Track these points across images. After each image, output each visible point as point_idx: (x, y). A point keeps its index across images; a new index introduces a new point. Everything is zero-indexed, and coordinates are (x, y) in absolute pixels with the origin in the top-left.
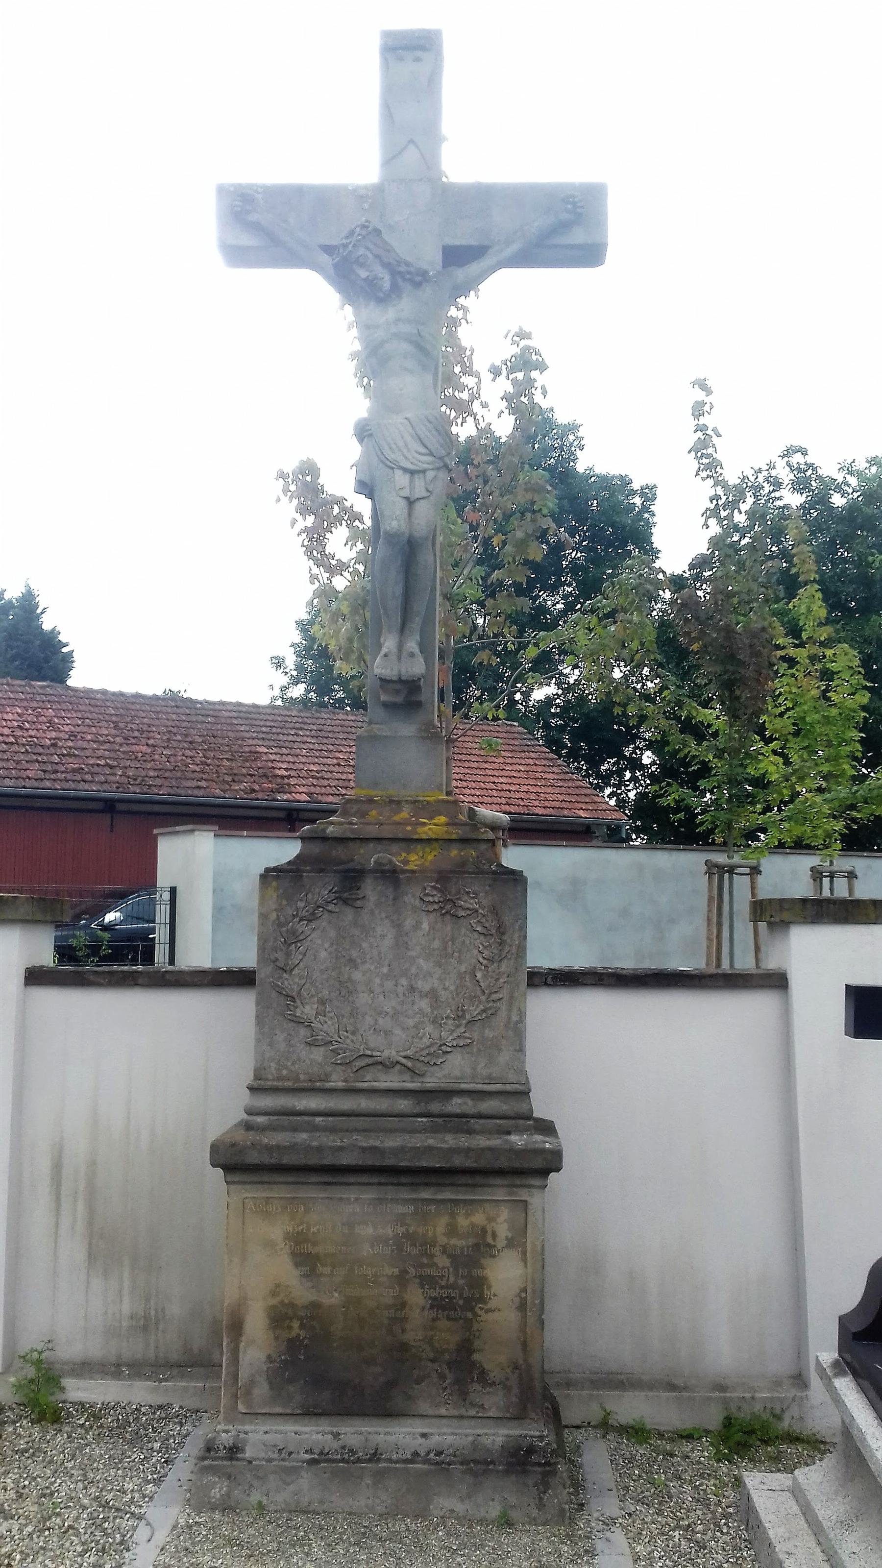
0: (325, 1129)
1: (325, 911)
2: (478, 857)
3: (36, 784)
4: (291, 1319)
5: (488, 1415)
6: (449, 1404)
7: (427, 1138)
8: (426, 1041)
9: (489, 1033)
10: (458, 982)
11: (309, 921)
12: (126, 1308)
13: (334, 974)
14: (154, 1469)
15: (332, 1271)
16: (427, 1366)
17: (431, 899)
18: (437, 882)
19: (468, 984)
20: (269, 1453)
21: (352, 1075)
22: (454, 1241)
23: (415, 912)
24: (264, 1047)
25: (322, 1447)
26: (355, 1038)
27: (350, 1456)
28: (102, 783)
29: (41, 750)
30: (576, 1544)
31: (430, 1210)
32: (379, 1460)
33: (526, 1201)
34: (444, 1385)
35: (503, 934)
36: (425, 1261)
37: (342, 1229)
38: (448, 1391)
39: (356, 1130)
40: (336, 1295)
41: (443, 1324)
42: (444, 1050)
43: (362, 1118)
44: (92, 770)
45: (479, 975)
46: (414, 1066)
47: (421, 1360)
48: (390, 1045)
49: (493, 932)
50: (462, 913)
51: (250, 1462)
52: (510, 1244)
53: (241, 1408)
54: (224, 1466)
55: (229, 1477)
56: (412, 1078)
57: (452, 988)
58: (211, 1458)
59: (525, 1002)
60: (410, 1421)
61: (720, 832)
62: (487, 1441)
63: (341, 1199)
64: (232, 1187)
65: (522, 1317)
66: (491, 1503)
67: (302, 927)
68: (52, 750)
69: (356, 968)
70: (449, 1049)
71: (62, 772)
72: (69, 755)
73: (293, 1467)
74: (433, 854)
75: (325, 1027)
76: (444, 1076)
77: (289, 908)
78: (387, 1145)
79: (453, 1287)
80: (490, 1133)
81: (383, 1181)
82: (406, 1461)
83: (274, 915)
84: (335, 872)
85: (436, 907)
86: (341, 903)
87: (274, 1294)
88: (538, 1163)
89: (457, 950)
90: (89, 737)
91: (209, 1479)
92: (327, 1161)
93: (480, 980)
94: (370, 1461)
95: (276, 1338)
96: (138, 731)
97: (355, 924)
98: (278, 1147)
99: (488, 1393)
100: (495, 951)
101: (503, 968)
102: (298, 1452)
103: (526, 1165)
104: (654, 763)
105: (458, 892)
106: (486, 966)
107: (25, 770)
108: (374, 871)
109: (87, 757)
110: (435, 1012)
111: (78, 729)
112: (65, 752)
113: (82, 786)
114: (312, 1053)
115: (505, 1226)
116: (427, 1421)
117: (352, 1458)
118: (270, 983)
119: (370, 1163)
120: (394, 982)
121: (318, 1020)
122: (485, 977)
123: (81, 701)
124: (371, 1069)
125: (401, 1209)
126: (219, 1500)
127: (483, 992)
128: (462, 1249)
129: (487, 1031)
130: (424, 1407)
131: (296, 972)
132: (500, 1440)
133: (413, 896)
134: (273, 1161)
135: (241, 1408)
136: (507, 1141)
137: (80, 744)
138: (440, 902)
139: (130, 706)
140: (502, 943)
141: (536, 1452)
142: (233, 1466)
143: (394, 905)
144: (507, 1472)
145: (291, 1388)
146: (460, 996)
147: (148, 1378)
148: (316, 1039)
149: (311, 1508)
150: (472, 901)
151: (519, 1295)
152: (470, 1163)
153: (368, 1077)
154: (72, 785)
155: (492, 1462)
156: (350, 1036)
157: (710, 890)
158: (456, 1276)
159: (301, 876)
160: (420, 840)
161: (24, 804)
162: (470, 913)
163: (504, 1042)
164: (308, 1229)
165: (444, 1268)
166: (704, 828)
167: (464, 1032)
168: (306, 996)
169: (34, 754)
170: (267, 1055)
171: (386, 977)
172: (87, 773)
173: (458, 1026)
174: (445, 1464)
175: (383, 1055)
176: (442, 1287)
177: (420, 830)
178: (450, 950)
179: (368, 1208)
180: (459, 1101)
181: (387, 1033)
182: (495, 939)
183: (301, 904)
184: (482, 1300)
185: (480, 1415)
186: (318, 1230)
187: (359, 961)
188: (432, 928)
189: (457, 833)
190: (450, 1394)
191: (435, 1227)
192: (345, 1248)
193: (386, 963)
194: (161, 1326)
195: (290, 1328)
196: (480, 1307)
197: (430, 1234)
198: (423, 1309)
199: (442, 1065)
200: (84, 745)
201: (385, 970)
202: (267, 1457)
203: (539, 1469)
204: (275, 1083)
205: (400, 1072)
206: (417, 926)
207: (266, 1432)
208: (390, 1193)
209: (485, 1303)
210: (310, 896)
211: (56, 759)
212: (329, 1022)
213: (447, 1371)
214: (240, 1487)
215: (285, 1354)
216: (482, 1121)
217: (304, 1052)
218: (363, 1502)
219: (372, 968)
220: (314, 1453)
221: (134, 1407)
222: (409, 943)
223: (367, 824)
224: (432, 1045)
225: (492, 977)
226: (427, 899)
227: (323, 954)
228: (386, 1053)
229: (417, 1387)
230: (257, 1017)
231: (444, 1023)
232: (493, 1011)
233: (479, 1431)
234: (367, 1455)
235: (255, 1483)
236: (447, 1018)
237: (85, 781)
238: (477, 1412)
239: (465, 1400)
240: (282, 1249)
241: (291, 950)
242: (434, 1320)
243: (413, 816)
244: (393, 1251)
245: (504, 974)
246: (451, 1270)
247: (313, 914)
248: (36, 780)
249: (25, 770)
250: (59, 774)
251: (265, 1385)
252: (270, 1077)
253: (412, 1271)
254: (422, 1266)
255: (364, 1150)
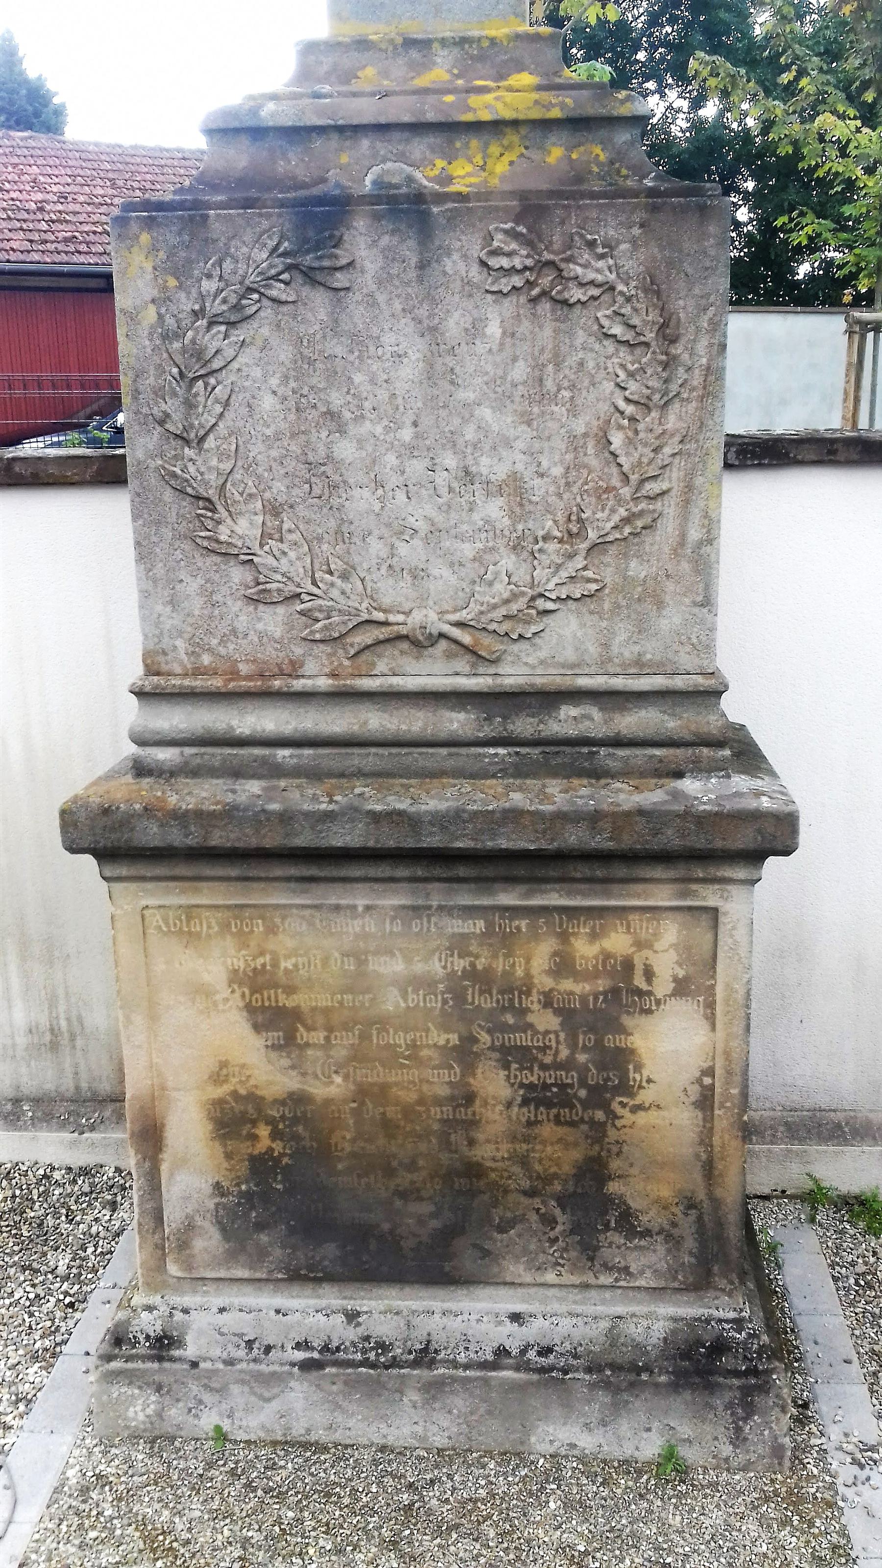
0: (296, 772)
1: (265, 302)
2: (612, 163)
3: (22, 257)
4: (254, 1123)
5: (637, 1284)
6: (563, 1266)
7: (508, 788)
8: (501, 589)
9: (636, 569)
10: (569, 457)
11: (231, 324)
12: (20, 1017)
13: (295, 448)
14: (49, 1324)
15: (327, 1039)
16: (519, 1203)
17: (505, 262)
18: (517, 220)
19: (594, 462)
20: (230, 1347)
21: (347, 663)
22: (567, 985)
23: (470, 296)
24: (159, 608)
25: (326, 1338)
26: (347, 587)
27: (377, 1355)
28: (101, 254)
29: (26, 216)
30: (811, 1524)
31: (518, 928)
32: (432, 1364)
33: (716, 910)
34: (552, 1234)
35: (674, 341)
36: (510, 1019)
37: (343, 962)
38: (561, 1243)
39: (360, 774)
40: (338, 1079)
41: (547, 1130)
42: (541, 608)
43: (373, 750)
44: (88, 239)
45: (617, 440)
46: (477, 642)
47: (506, 1191)
48: (423, 600)
49: (650, 336)
50: (576, 294)
51: (195, 1365)
52: (681, 988)
53: (173, 1269)
54: (145, 1371)
55: (159, 1389)
56: (473, 665)
57: (557, 471)
58: (122, 1357)
59: (719, 496)
60: (489, 1291)
61: (865, 276)
62: (635, 1330)
63: (337, 908)
64: (118, 887)
65: (704, 1120)
66: (645, 1435)
67: (213, 340)
68: (39, 216)
69: (342, 430)
70: (550, 606)
71: (52, 242)
72: (58, 221)
73: (273, 1374)
74: (506, 159)
75: (284, 563)
76: (542, 662)
77: (182, 295)
78: (424, 807)
79: (568, 1065)
80: (642, 775)
81: (420, 873)
82: (484, 1365)
83: (151, 314)
84: (282, 204)
85: (517, 281)
86: (299, 279)
87: (218, 1078)
88: (744, 839)
89: (566, 384)
90: (81, 199)
91: (122, 1390)
92: (302, 841)
93: (618, 452)
94: (415, 1364)
95: (228, 1156)
96: (140, 189)
97: (334, 327)
98: (199, 814)
99: (636, 1248)
100: (654, 383)
101: (672, 421)
102: (283, 1347)
103: (719, 844)
104: (751, 220)
105: (569, 245)
106: (632, 419)
107: (8, 240)
108: (373, 199)
109: (81, 223)
110: (520, 527)
111: (68, 189)
112: (54, 217)
113: (77, 258)
114: (260, 619)
115: (672, 956)
116: (520, 1291)
117: (382, 1359)
118: (157, 469)
119: (391, 844)
120: (427, 462)
121: (267, 548)
122: (629, 442)
123: (70, 154)
124: (389, 650)
125: (457, 926)
126: (144, 1423)
127: (626, 478)
128: (584, 999)
129: (633, 564)
130: (516, 1270)
131: (210, 443)
132: (659, 1329)
133: (465, 257)
134: (191, 841)
135: (173, 1269)
136: (676, 795)
137: (72, 207)
138: (526, 268)
139: (128, 159)
140: (669, 364)
141: (730, 1349)
142: (165, 1370)
143: (420, 280)
144: (675, 1387)
145: (264, 1238)
146: (575, 489)
147: (63, 1125)
148: (265, 590)
149: (313, 1438)
150: (601, 264)
151: (699, 1081)
152: (600, 842)
153: (381, 666)
154: (64, 258)
155: (647, 1369)
156: (339, 582)
157: (849, 354)
158: (573, 1046)
159: (205, 217)
160: (477, 127)
161: (15, 284)
162: (596, 292)
163: (670, 586)
164: (275, 964)
165: (547, 1032)
166: (845, 271)
167: (585, 568)
168: (237, 497)
169: (18, 220)
170: (168, 624)
171: (411, 450)
172: (80, 243)
173: (571, 556)
174: (558, 1370)
175: (409, 620)
176: (544, 1067)
177: (474, 100)
178: (549, 384)
179: (391, 923)
180: (574, 711)
181: (417, 574)
182: (654, 353)
183: (209, 286)
184: (625, 1088)
185: (622, 1283)
186: (296, 966)
187: (347, 415)
188: (509, 334)
189: (562, 106)
190: (566, 1250)
191: (528, 960)
192: (350, 997)
193: (408, 419)
194: (79, 1043)
195: (254, 1138)
196: (621, 1103)
197: (520, 972)
198: (509, 1105)
199: (537, 640)
200: (77, 207)
201: (407, 434)
202: (225, 1355)
203: (736, 1382)
204: (187, 682)
205: (449, 656)
206: (475, 330)
207: (222, 1310)
208: (437, 895)
209: (632, 1095)
210: (228, 265)
211: (44, 226)
212: (292, 555)
213: (558, 1212)
214: (181, 1405)
215: (247, 1182)
216: (621, 752)
217: (243, 618)
218: (406, 1431)
219: (379, 430)
220: (313, 1349)
221: (41, 1172)
222: (457, 370)
223: (354, 95)
224: (515, 596)
225: (646, 445)
226: (494, 262)
227: (268, 402)
228: (417, 618)
229: (499, 1236)
230: (138, 544)
231: (540, 550)
232: (647, 520)
233: (620, 1310)
234: (410, 1352)
235: (207, 1397)
236: (545, 538)
237: (80, 252)
238: (617, 1280)
239: (591, 1259)
240: (226, 1000)
241: (196, 395)
242: (530, 1124)
243: (458, 76)
244: (445, 1002)
245: (672, 435)
246: (562, 1036)
247: (237, 307)
248: (22, 252)
249: (8, 240)
250: (48, 245)
251: (215, 1235)
252: (178, 670)
253: (485, 1038)
254: (505, 1028)
255: (376, 817)
